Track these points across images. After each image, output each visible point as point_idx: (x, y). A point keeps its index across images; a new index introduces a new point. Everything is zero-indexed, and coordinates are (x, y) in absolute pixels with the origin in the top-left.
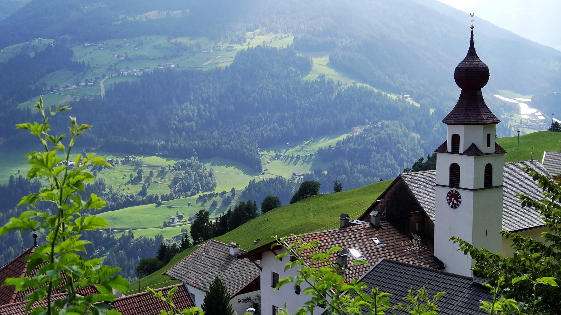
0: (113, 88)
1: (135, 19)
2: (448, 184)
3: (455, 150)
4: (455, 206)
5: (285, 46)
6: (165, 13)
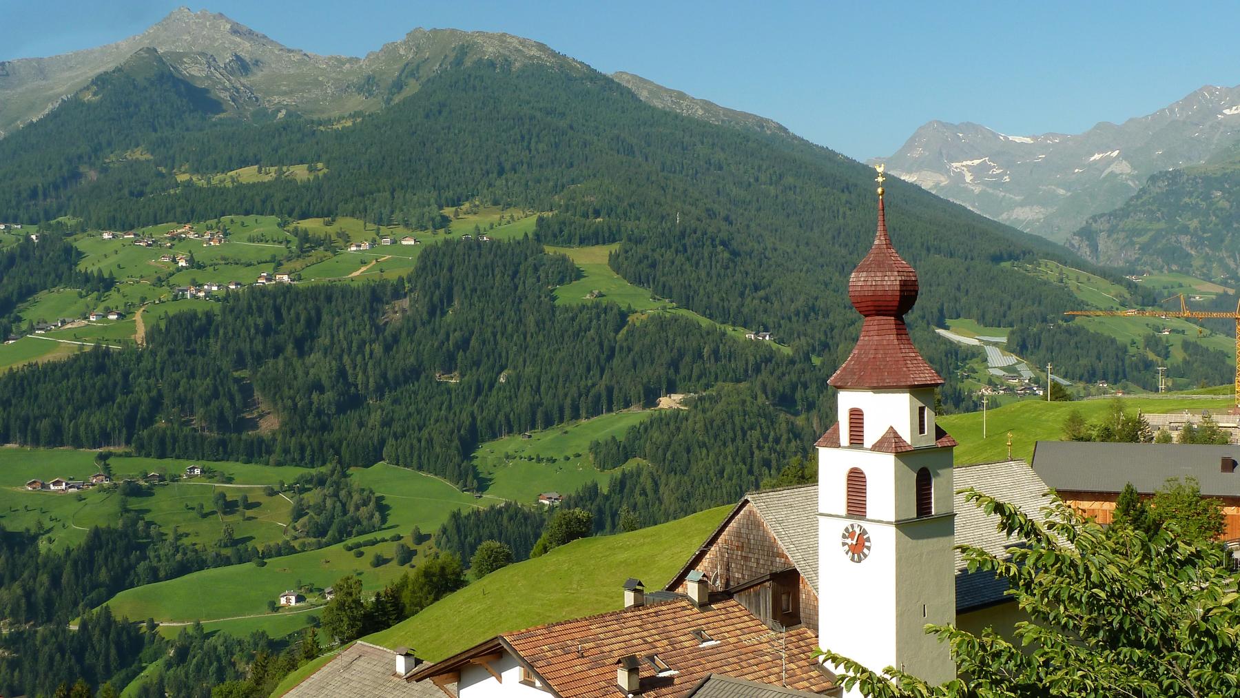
0: (163, 326)
1: (209, 182)
2: (844, 512)
3: (856, 440)
4: (1235, 464)
5: (520, 237)
6: (273, 169)
